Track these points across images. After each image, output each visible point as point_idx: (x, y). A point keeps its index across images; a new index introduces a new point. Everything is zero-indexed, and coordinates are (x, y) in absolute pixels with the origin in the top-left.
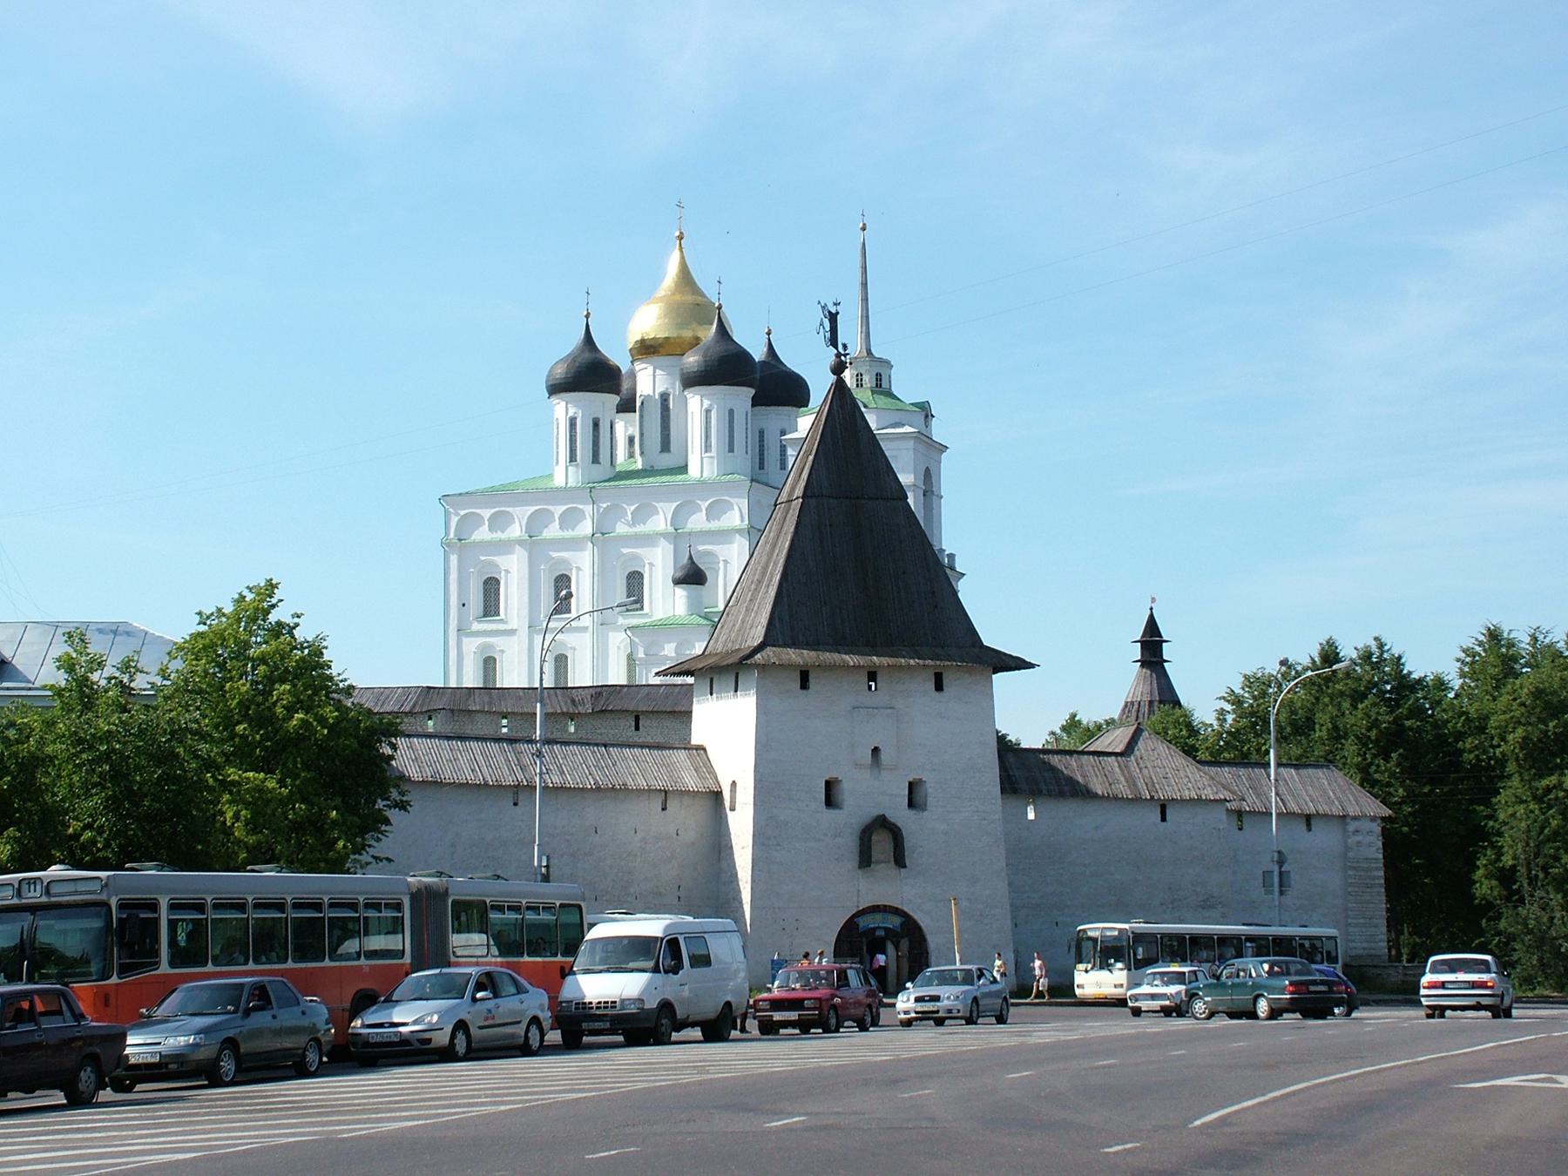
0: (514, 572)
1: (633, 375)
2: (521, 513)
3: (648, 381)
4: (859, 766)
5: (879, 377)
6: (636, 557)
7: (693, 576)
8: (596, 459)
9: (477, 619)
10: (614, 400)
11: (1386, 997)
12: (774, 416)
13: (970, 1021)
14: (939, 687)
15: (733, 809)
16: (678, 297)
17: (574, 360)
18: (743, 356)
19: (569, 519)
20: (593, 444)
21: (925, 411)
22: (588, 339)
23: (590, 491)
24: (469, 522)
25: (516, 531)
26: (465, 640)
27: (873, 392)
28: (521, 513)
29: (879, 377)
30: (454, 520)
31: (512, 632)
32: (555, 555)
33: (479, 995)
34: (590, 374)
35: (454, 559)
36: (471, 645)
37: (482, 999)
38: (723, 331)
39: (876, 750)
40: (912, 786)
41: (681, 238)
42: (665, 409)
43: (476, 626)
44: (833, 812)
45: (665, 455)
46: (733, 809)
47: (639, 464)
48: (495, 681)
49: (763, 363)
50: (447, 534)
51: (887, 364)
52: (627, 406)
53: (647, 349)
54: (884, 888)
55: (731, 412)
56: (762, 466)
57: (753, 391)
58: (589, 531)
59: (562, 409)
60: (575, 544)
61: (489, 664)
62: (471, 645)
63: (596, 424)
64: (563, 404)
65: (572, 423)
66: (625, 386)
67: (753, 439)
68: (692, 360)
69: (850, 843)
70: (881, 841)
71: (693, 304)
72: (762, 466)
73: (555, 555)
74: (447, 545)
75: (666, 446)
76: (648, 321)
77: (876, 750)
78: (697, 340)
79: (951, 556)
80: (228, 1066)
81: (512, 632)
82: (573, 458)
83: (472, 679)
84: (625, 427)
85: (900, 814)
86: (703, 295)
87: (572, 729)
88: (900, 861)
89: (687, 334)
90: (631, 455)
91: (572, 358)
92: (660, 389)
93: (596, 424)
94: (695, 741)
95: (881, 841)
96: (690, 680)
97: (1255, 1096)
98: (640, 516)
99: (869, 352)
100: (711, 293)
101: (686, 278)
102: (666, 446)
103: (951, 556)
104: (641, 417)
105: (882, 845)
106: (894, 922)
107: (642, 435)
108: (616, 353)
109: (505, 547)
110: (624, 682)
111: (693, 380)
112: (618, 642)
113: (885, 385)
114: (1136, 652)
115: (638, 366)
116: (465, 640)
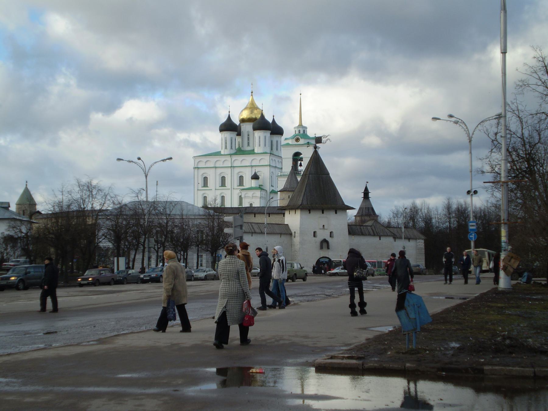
5: (304, 131)
7: (255, 177)
11: (140, 301)
12: (276, 138)
14: (336, 213)
18: (267, 122)
22: (229, 118)
29: (304, 131)
44: (314, 238)
51: (306, 128)
55: (265, 137)
56: (272, 150)
57: (270, 132)
67: (270, 144)
69: (318, 244)
70: (325, 244)
71: (252, 107)
72: (272, 150)
80: (21, 286)
84: (238, 139)
85: (328, 239)
88: (328, 248)
95: (325, 244)
97: (134, 371)
105: (325, 245)
106: (327, 260)
112: (236, 193)
114: (362, 195)
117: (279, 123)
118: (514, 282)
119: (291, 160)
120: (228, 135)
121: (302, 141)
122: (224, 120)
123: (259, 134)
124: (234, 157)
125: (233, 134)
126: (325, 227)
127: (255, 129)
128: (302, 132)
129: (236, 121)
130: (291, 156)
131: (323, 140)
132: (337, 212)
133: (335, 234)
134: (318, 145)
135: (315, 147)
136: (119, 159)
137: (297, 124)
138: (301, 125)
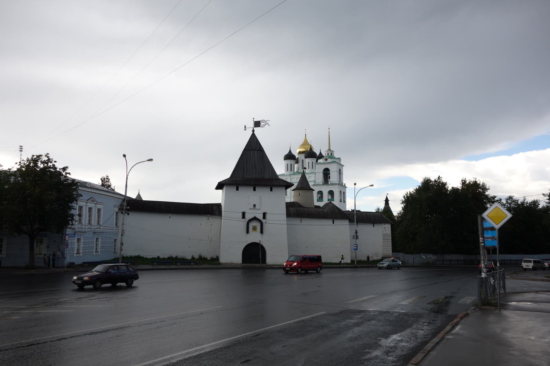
4: (250, 209)
18: (315, 154)
39: (255, 205)
52: (297, 162)
54: (254, 237)
63: (291, 165)
77: (255, 205)
84: (296, 166)
118: (43, 250)
119: (322, 174)
120: (289, 162)
121: (329, 160)
122: (287, 152)
123: (307, 160)
124: (292, 177)
125: (293, 162)
126: (257, 207)
127: (306, 157)
128: (330, 154)
129: (295, 153)
130: (322, 170)
131: (262, 124)
133: (267, 216)
134: (255, 129)
135: (253, 131)
136: (151, 160)
137: (327, 148)
138: (329, 149)
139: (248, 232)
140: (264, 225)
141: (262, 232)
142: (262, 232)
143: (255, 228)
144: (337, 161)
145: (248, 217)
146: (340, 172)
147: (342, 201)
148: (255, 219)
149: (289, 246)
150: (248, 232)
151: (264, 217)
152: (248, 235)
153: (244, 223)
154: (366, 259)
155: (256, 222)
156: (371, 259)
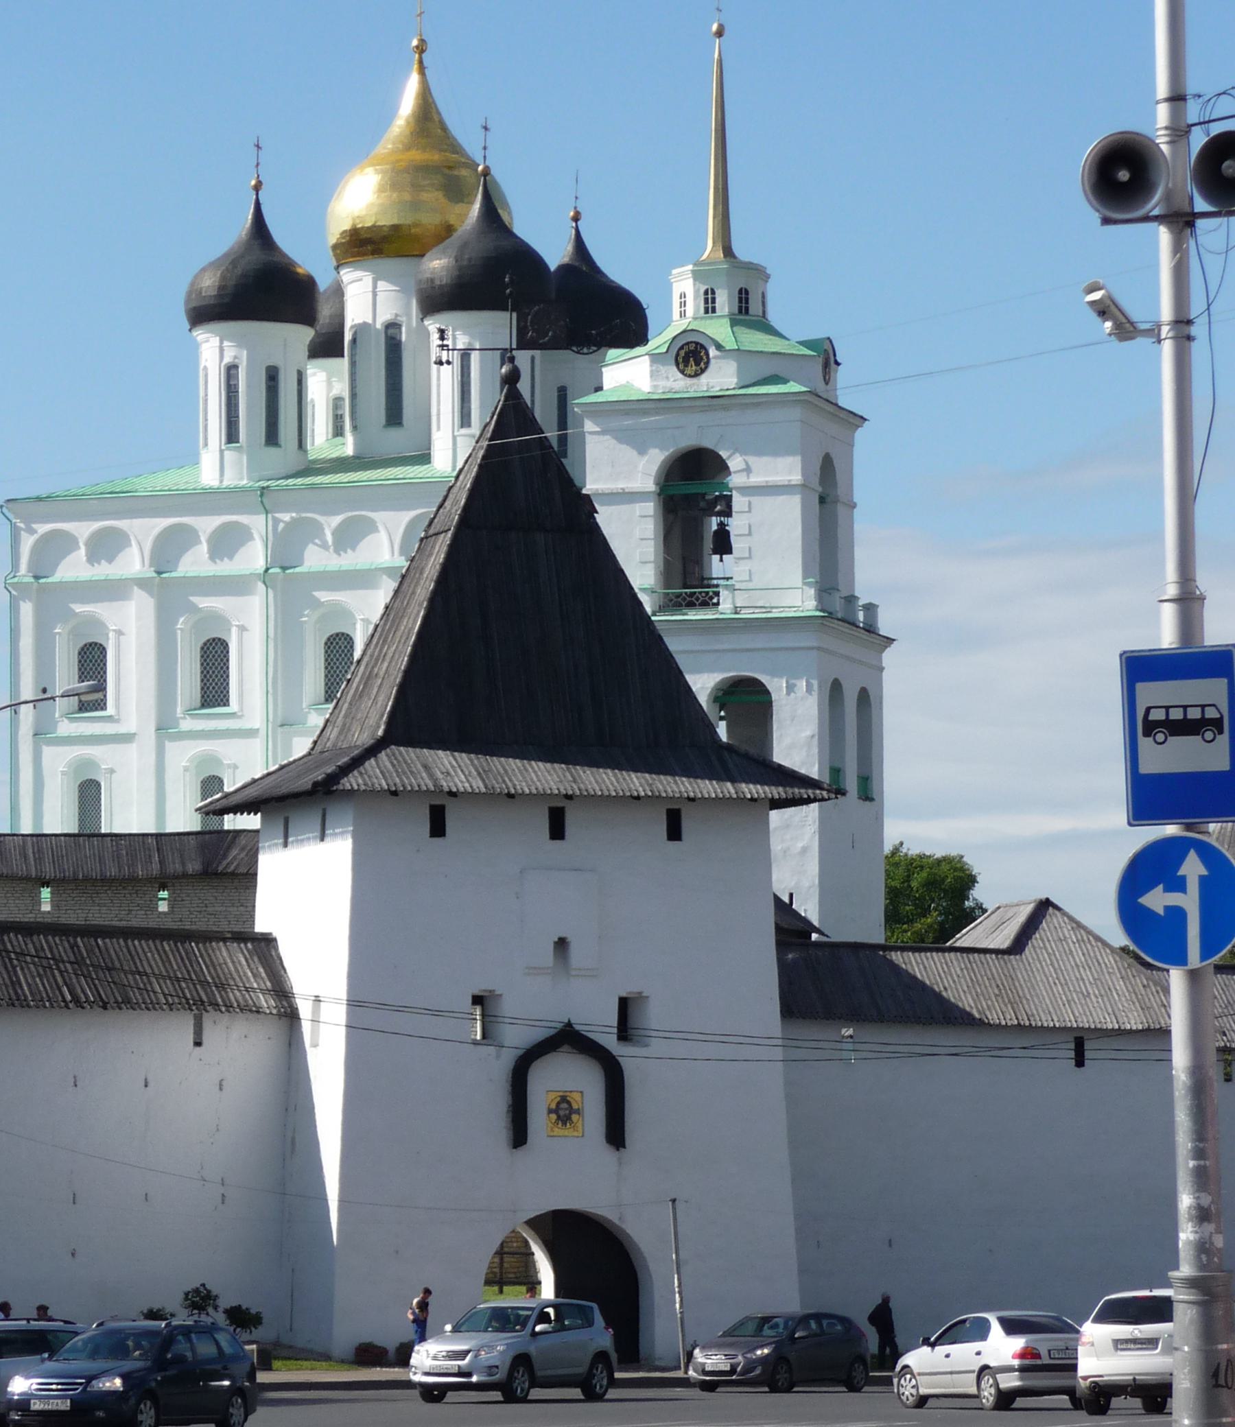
0: (130, 633)
1: (338, 292)
2: (144, 531)
3: (365, 299)
5: (743, 298)
6: (217, 618)
8: (272, 437)
9: (189, 711)
10: (302, 335)
13: (511, 1396)
15: (315, 1045)
16: (417, 156)
17: (234, 263)
18: (526, 258)
19: (226, 543)
20: (271, 412)
21: (826, 357)
23: (264, 498)
24: (52, 549)
25: (133, 563)
26: (48, 751)
27: (734, 323)
28: (144, 531)
30: (27, 543)
31: (127, 738)
32: (79, 608)
33: (538, 1328)
34: (263, 288)
35: (27, 610)
36: (58, 760)
37: (541, 1333)
38: (492, 215)
39: (562, 944)
40: (624, 1003)
41: (421, 49)
42: (394, 348)
43: (187, 724)
45: (394, 433)
46: (315, 1045)
47: (348, 446)
48: (19, 828)
49: (563, 268)
50: (15, 565)
51: (758, 272)
52: (328, 345)
53: (363, 245)
54: (572, 1171)
58: (259, 564)
59: (213, 348)
60: (236, 586)
61: (89, 794)
62: (58, 760)
63: (272, 376)
64: (215, 341)
65: (231, 371)
66: (325, 312)
68: (437, 264)
71: (438, 157)
73: (79, 608)
74: (17, 593)
75: (394, 416)
76: (360, 197)
77: (562, 944)
78: (448, 230)
79: (870, 608)
81: (127, 738)
82: (232, 436)
83: (59, 818)
84: (324, 383)
86: (455, 148)
87: (163, 907)
89: (430, 220)
90: (338, 431)
91: (233, 260)
92: (384, 317)
93: (272, 376)
94: (260, 927)
96: (251, 821)
98: (347, 538)
99: (728, 252)
100: (470, 140)
101: (427, 116)
102: (394, 416)
103: (870, 608)
104: (353, 364)
107: (353, 396)
108: (308, 252)
109: (114, 590)
110: (73, 828)
111: (436, 301)
113: (755, 307)
115: (347, 275)
116: (48, 751)
117: (616, 267)
132: (570, 829)
133: (654, 1016)
139: (519, 1135)
140: (628, 1066)
141: (616, 1135)
142: (616, 1135)
143: (564, 1112)
144: (816, 399)
145: (517, 1037)
146: (828, 498)
147: (851, 784)
148: (568, 1038)
149: (808, 1227)
150: (519, 1135)
151: (624, 1033)
152: (520, 1152)
153: (499, 1065)
154: (505, 1288)
155: (586, 1062)
156: (496, 1288)
